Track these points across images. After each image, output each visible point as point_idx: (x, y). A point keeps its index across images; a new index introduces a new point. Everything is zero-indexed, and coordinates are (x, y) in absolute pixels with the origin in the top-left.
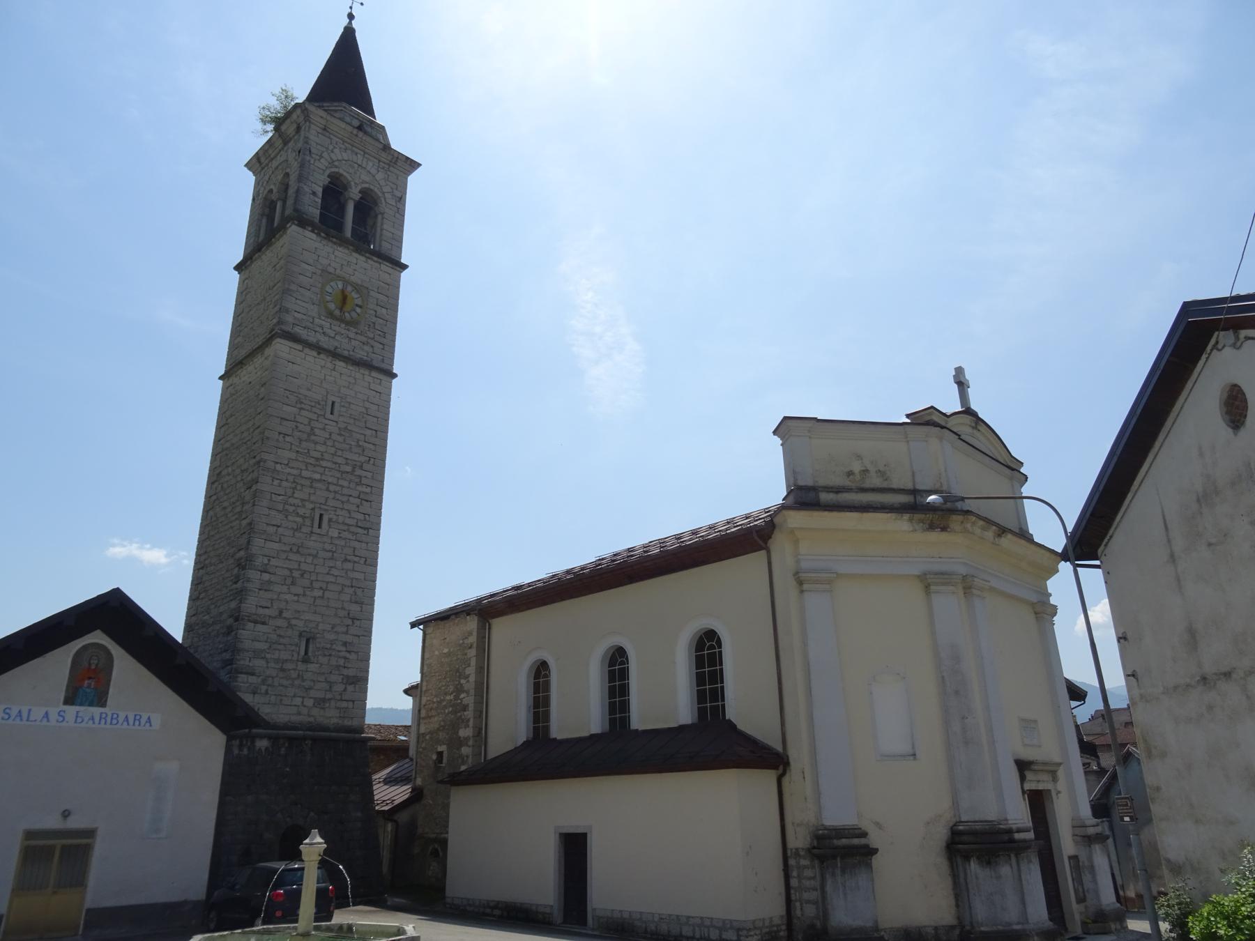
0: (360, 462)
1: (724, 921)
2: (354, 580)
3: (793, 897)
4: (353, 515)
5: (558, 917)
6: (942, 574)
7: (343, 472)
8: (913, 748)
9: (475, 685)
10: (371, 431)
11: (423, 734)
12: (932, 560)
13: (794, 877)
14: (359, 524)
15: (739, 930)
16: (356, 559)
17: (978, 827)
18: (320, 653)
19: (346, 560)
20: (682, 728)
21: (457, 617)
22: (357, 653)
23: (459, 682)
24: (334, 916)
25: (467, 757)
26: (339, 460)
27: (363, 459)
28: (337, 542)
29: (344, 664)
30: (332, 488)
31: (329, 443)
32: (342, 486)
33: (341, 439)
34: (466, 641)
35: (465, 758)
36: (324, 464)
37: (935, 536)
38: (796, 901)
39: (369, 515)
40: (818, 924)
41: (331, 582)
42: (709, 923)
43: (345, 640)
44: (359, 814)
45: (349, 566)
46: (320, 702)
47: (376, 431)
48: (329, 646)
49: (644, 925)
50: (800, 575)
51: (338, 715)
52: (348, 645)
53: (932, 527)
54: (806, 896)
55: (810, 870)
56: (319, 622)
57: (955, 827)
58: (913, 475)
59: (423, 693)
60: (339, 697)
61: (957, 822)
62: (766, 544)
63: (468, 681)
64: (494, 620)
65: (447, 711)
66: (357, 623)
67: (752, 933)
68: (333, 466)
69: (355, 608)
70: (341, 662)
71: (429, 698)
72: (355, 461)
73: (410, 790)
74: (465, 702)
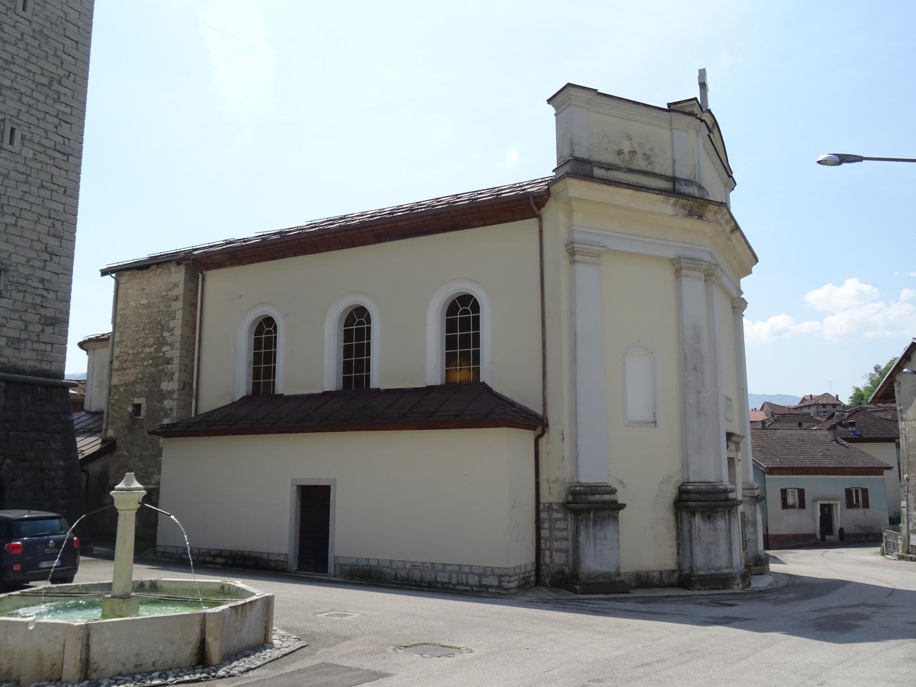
0: (58, 75)
1: (485, 568)
2: (52, 210)
3: (543, 546)
4: (50, 135)
5: (293, 563)
6: (694, 259)
7: (38, 84)
8: (654, 414)
9: (182, 338)
10: (70, 41)
11: (115, 386)
12: (685, 245)
13: (545, 529)
14: (58, 147)
15: (501, 576)
16: (55, 187)
17: (703, 487)
18: (13, 287)
19: (42, 186)
20: (430, 389)
21: (158, 268)
22: (56, 292)
23: (161, 334)
24: (80, 568)
25: (171, 410)
26: (34, 68)
27: (62, 72)
28: (32, 164)
29: (42, 302)
30: (25, 99)
31: (22, 45)
32: (38, 101)
33: (35, 43)
34: (170, 293)
35: (169, 412)
36: (15, 68)
37: (692, 224)
38: (546, 549)
39: (69, 139)
40: (567, 571)
41: (26, 209)
42: (468, 571)
43: (42, 277)
44: (61, 463)
45: (46, 194)
46: (14, 342)
47: (77, 42)
48: (23, 281)
49: (394, 572)
50: (575, 245)
51: (35, 357)
52: (45, 282)
53: (690, 214)
54: (556, 545)
55: (563, 522)
56: (12, 253)
57: (682, 487)
58: (674, 162)
59: (116, 344)
60: (36, 339)
61: (684, 483)
62: (539, 210)
63: (173, 334)
64: (208, 272)
65: (145, 364)
66: (56, 259)
67: (513, 579)
68: (27, 74)
69: (53, 242)
70: (38, 300)
71: (123, 350)
72: (53, 73)
73: (100, 441)
74: (168, 355)
